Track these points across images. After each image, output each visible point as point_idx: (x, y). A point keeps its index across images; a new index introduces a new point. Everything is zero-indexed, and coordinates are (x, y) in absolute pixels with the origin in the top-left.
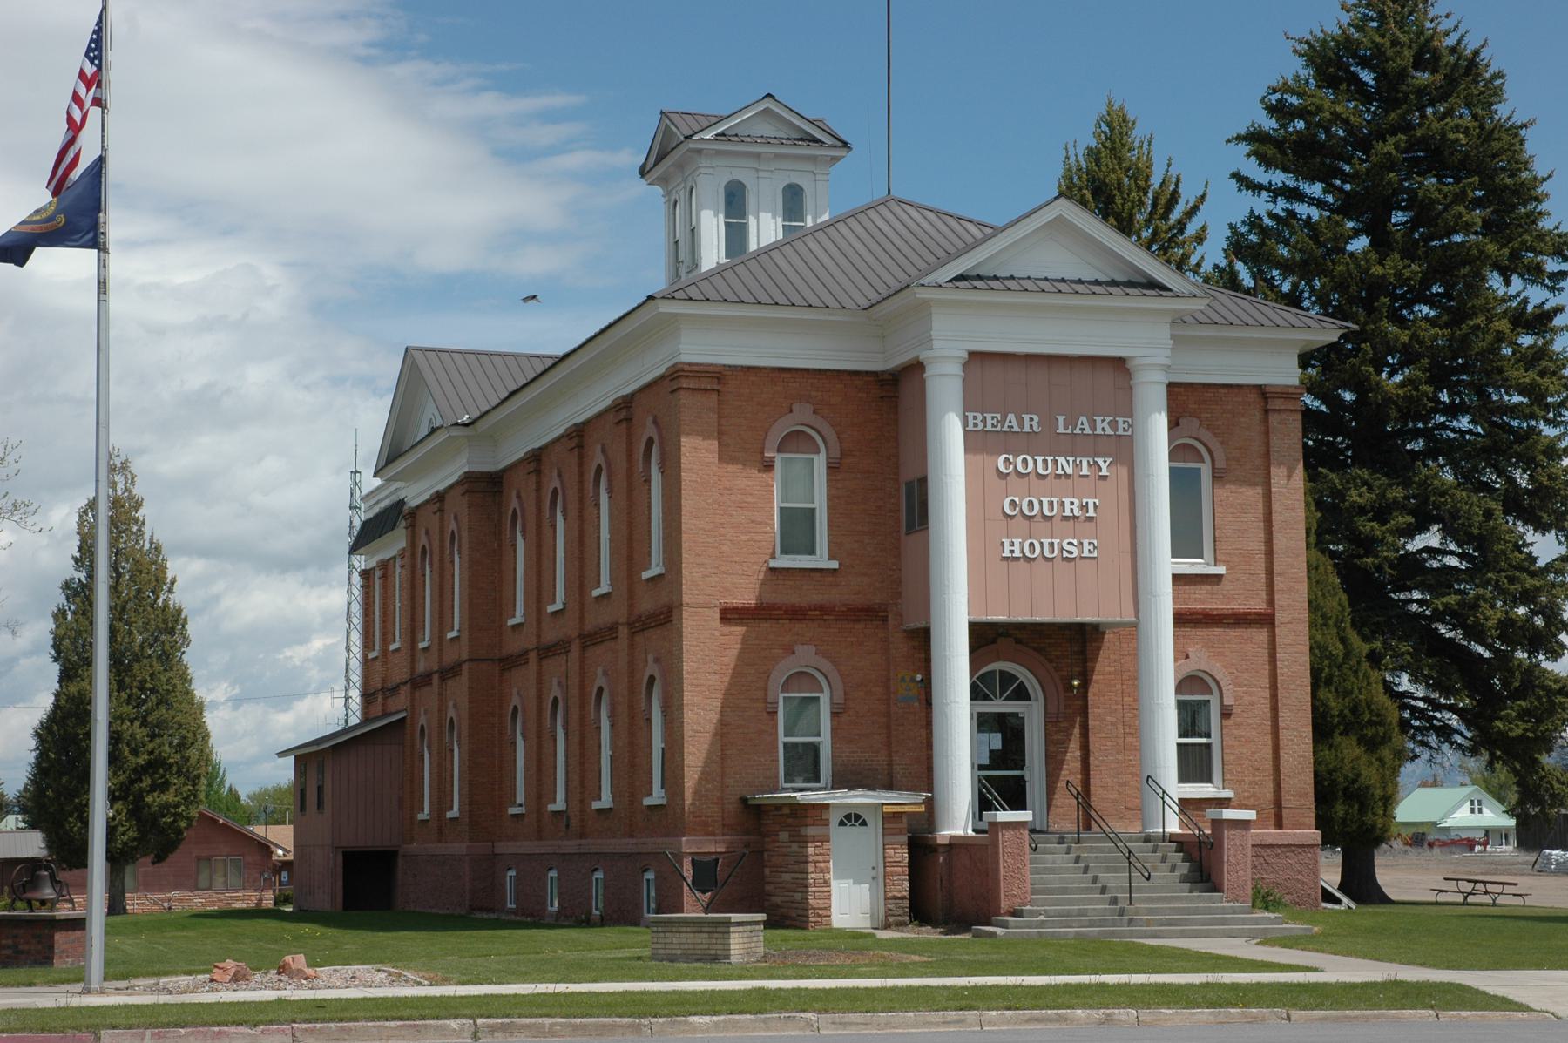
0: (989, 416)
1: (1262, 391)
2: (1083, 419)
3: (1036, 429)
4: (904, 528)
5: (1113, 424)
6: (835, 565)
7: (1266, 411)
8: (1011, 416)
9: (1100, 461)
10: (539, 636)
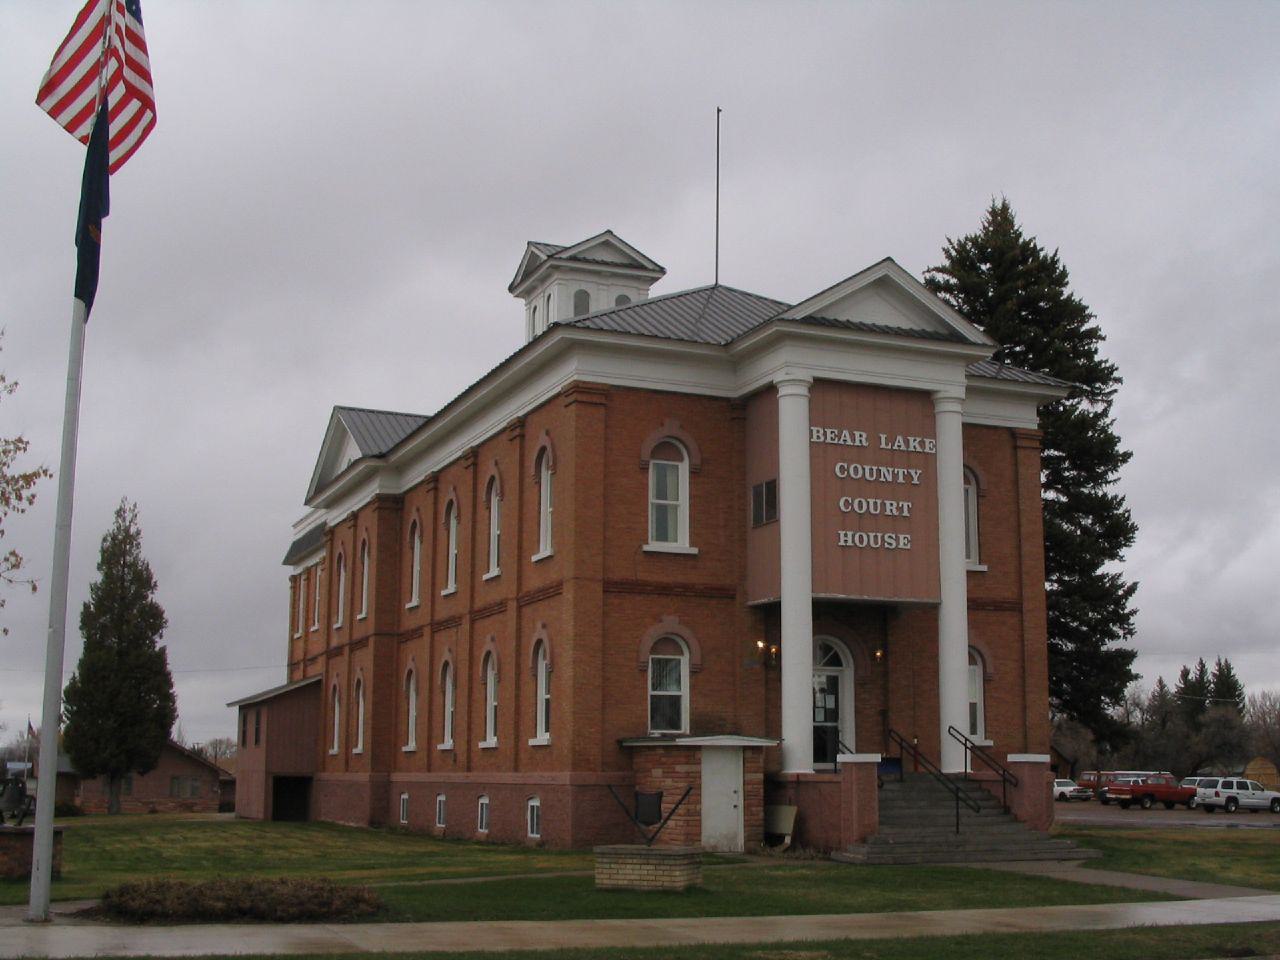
0: (828, 431)
1: (1013, 433)
2: (900, 438)
3: (864, 444)
4: (751, 523)
5: (922, 444)
6: (695, 551)
7: (1015, 448)
9: (913, 472)
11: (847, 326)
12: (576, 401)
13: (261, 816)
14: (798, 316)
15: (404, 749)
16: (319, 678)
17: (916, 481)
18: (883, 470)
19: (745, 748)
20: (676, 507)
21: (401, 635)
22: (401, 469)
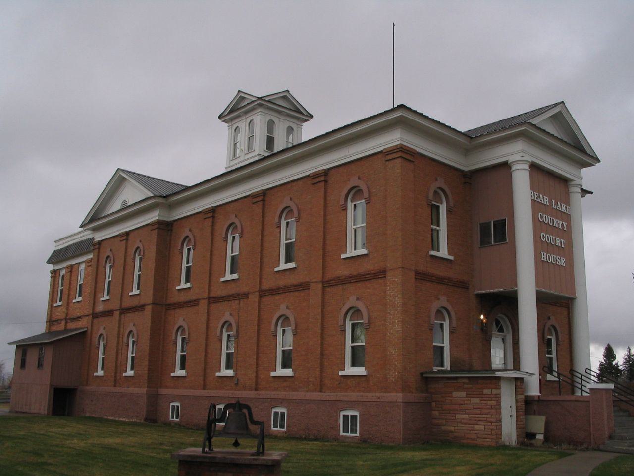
10: (209, 293)
12: (400, 157)
13: (46, 412)
15: (124, 375)
16: (86, 329)
21: (169, 305)
22: (172, 207)
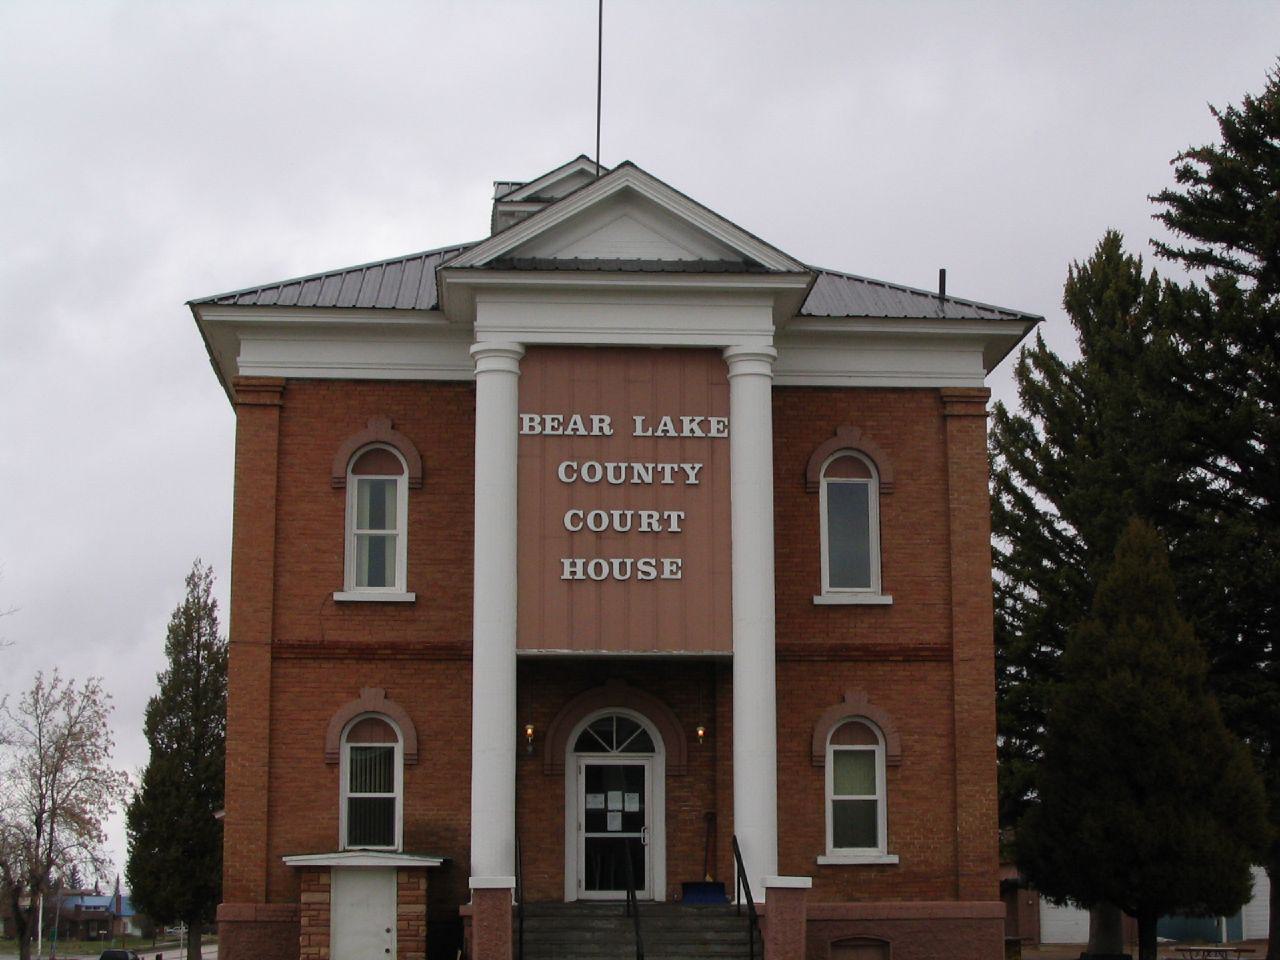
0: (548, 418)
3: (607, 431)
5: (705, 425)
7: (945, 418)
8: (577, 418)
9: (687, 467)
11: (576, 267)
14: (479, 261)
17: (692, 480)
18: (638, 467)
19: (400, 869)
20: (394, 538)
